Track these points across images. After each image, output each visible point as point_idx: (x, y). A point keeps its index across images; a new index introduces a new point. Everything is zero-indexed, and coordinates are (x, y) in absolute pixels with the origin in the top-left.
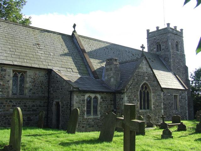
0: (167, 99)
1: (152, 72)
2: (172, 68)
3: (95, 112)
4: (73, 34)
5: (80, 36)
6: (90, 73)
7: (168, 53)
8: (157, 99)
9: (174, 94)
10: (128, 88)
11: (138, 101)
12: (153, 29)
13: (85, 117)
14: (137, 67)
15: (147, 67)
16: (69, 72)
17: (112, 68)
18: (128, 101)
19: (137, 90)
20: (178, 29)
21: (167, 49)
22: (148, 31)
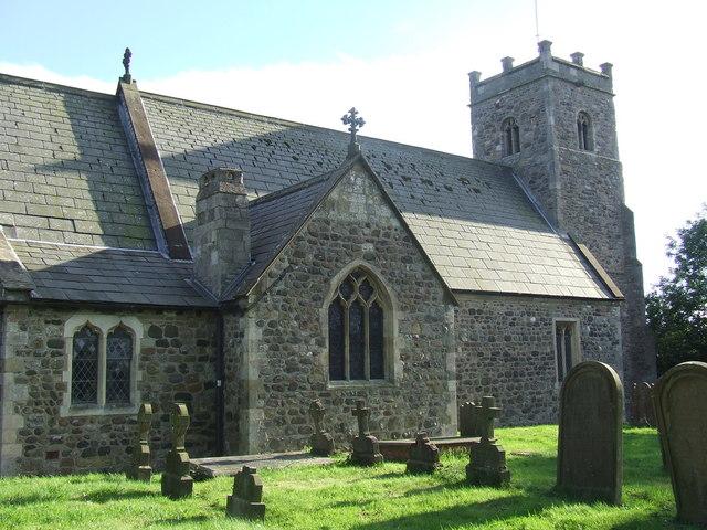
0: (525, 339)
1: (395, 223)
2: (560, 217)
3: (120, 388)
4: (120, 89)
5: (147, 96)
6: (159, 235)
7: (545, 157)
8: (422, 337)
9: (555, 319)
10: (263, 289)
11: (320, 344)
12: (491, 69)
13: (65, 411)
14: (323, 202)
15: (371, 202)
16: (52, 234)
17: (213, 210)
18: (266, 347)
19: (318, 299)
20: (592, 64)
21: (542, 142)
22: (474, 76)
